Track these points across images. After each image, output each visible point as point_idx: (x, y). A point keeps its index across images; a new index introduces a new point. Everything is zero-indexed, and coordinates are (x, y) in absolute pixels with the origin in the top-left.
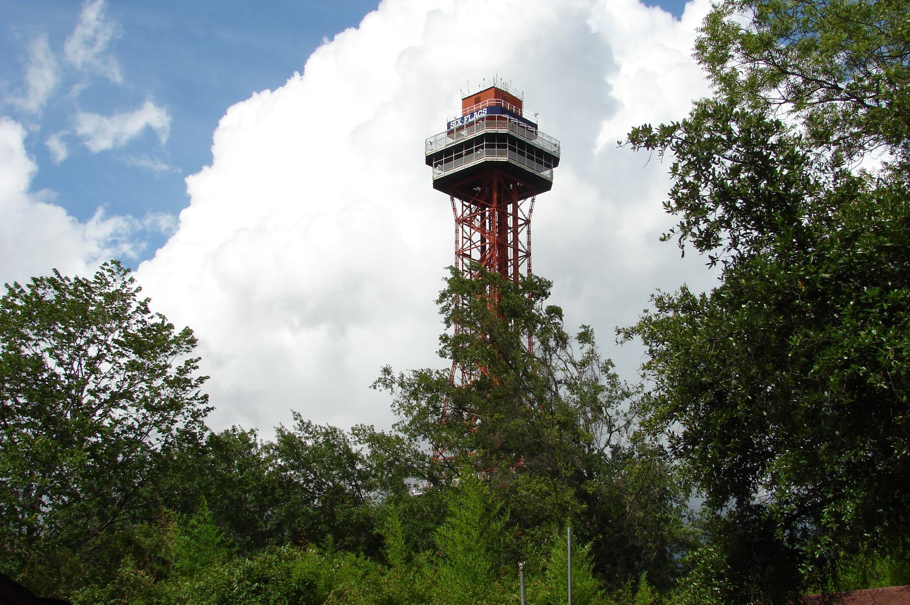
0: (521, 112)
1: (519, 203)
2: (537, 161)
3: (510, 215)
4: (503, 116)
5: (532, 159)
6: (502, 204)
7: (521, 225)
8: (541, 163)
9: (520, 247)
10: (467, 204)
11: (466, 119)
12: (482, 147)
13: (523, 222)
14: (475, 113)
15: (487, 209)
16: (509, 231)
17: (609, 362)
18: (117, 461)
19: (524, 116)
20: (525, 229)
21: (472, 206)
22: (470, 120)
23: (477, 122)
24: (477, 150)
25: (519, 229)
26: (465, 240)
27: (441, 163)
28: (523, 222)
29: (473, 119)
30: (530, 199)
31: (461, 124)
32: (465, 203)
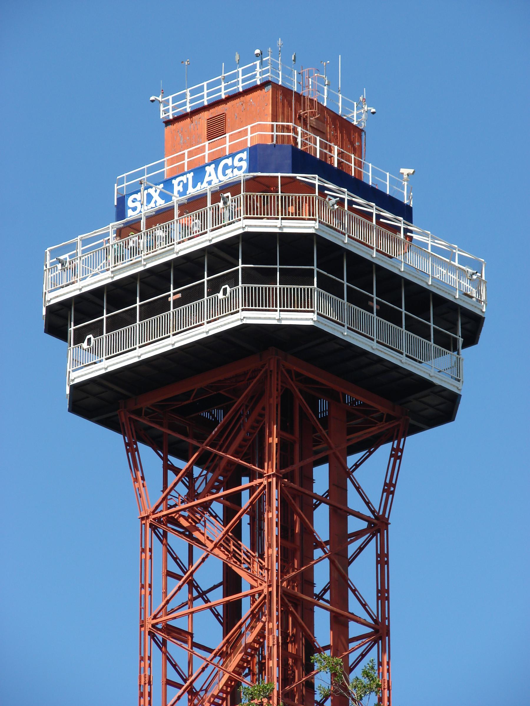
0: (359, 164)
1: (351, 460)
2: (412, 326)
3: (321, 500)
4: (299, 176)
5: (395, 318)
6: (296, 466)
7: (358, 534)
8: (423, 332)
9: (354, 606)
10: (183, 465)
11: (178, 188)
12: (232, 280)
13: (364, 525)
14: (210, 169)
15: (245, 482)
16: (318, 553)
17: (376, 696)
18: (386, 589)
19: (328, 506)
20: (371, 549)
21: (197, 471)
22: (192, 191)
23: (216, 196)
24: (214, 287)
25: (352, 548)
26: (173, 584)
27: (97, 330)
28: (364, 525)
29: (203, 187)
30: (385, 449)
31: (161, 203)
32: (174, 461)
